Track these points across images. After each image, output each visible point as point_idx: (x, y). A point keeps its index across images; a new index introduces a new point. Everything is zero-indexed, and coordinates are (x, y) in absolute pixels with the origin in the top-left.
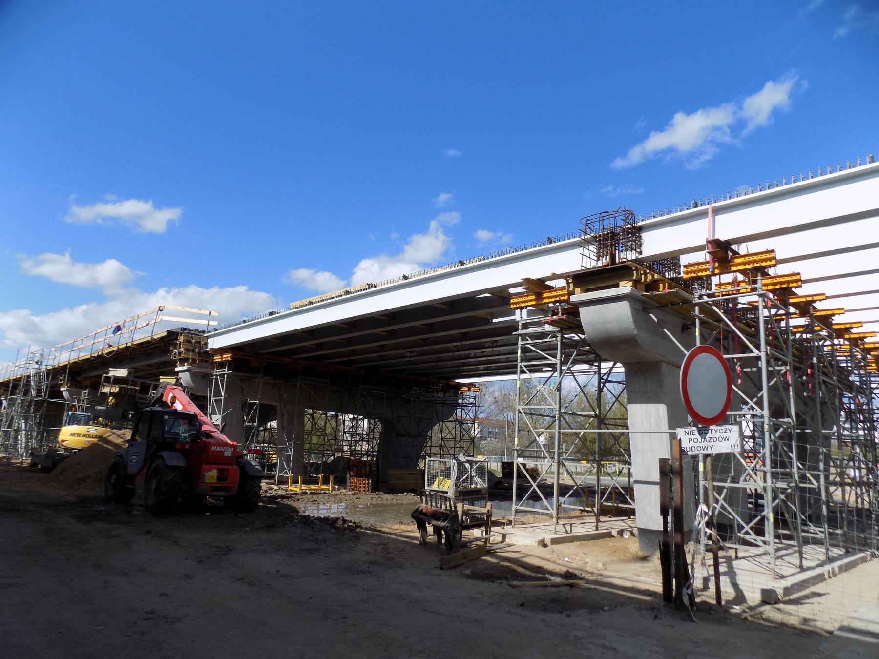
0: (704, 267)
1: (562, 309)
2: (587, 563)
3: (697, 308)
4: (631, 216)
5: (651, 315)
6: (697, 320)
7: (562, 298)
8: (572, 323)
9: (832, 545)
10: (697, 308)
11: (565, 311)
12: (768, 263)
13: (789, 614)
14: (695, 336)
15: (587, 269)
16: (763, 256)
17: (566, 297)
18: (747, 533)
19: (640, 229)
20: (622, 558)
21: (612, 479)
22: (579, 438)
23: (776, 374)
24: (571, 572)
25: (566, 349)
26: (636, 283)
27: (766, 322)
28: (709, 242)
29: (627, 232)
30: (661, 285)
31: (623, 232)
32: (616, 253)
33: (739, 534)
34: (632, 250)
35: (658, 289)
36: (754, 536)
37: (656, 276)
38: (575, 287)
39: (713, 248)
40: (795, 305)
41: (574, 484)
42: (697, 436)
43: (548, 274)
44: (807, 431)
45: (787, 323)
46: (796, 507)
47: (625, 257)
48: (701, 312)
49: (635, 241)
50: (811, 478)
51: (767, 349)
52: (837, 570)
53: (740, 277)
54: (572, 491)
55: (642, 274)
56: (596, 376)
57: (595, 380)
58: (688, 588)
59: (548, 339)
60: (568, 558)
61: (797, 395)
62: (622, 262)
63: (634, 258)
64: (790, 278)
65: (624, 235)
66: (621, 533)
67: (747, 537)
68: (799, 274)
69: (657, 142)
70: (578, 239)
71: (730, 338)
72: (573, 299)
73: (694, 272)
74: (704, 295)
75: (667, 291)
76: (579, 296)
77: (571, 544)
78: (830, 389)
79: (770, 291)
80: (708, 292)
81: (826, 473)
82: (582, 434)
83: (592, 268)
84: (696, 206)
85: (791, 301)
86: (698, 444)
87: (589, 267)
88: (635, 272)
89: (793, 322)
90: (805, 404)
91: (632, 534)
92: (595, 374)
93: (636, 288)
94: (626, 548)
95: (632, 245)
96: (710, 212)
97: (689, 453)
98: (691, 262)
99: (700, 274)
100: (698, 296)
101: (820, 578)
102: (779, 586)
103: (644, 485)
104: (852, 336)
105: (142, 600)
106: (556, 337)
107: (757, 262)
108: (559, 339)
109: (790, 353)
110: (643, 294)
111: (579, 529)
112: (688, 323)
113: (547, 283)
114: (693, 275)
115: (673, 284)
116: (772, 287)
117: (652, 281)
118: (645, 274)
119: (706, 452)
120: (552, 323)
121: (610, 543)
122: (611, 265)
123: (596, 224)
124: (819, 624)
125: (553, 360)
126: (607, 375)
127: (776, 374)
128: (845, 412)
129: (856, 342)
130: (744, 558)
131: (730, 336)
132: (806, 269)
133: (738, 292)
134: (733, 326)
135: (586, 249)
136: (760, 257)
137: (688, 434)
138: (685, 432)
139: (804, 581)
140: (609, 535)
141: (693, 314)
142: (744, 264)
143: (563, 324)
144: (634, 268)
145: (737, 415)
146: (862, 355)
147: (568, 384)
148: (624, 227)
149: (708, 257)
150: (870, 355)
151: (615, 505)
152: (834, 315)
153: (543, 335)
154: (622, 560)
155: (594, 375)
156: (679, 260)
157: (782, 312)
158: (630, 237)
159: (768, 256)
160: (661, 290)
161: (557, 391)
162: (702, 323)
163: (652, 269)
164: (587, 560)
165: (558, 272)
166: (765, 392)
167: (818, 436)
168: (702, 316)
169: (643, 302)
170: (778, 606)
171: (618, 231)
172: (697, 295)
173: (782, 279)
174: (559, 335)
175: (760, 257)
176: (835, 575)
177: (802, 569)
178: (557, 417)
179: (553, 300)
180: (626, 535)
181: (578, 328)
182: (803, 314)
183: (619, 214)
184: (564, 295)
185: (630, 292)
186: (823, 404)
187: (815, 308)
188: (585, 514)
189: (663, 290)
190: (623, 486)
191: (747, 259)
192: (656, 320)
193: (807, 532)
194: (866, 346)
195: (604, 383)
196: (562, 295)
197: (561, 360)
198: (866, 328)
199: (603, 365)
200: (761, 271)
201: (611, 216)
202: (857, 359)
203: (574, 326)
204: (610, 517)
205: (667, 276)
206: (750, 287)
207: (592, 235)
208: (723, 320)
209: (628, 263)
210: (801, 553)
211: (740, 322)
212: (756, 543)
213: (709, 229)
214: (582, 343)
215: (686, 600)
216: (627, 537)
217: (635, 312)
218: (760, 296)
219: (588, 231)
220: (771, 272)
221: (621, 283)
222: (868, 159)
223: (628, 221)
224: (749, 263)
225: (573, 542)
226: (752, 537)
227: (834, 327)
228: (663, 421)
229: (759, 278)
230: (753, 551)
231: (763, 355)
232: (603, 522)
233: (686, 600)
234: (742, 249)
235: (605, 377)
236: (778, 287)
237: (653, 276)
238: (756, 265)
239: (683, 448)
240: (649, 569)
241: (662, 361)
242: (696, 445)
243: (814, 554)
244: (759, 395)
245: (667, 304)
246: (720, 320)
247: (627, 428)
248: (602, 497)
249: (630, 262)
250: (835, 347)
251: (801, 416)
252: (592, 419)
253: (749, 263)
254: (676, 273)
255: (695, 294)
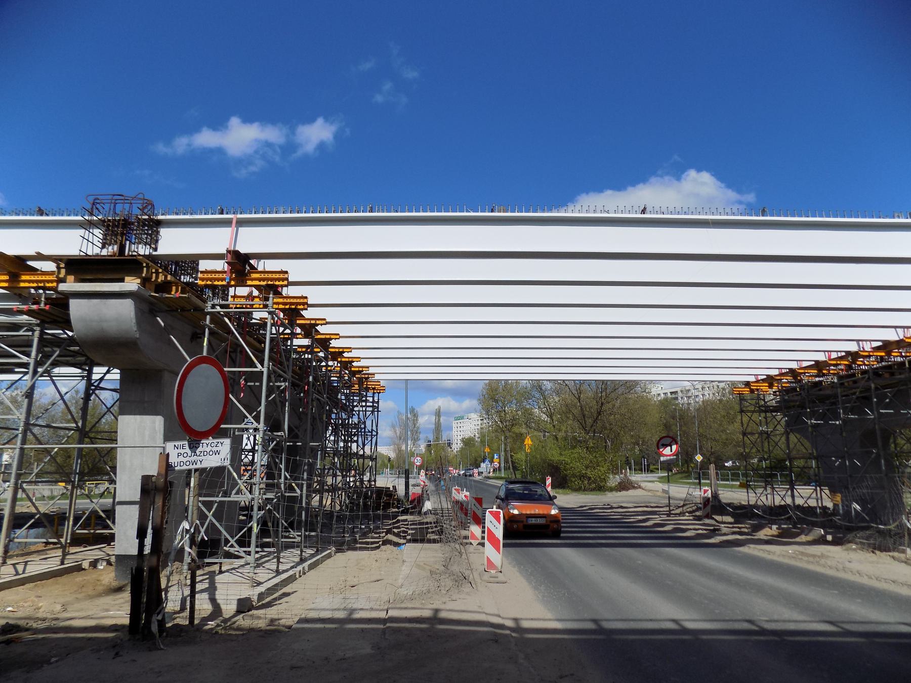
0: (221, 276)
1: (46, 299)
2: (39, 608)
3: (208, 317)
4: (150, 206)
5: (158, 318)
6: (207, 329)
7: (47, 285)
8: (57, 316)
9: (305, 547)
10: (208, 317)
11: (49, 300)
12: (281, 283)
13: (259, 618)
14: (203, 346)
15: (87, 255)
16: (277, 276)
17: (55, 284)
18: (232, 546)
19: (159, 223)
20: (90, 593)
21: (92, 502)
22: (51, 456)
23: (275, 389)
24: (11, 624)
25: (47, 346)
26: (145, 282)
27: (272, 340)
28: (229, 251)
29: (143, 223)
30: (174, 288)
31: (138, 223)
32: (125, 244)
33: (225, 548)
34: (146, 244)
35: (169, 292)
36: (237, 548)
37: (169, 278)
38: (68, 273)
39: (232, 258)
40: (301, 326)
41: (36, 512)
42: (188, 450)
43: (31, 252)
44: (298, 444)
45: (292, 342)
46: (279, 515)
47: (136, 250)
48: (212, 321)
49: (151, 235)
50: (296, 487)
51: (269, 365)
52: (306, 569)
53: (256, 293)
54: (33, 521)
55: (154, 273)
56: (84, 382)
57: (82, 385)
58: (158, 614)
59: (21, 333)
60: (12, 606)
61: (293, 410)
62: (132, 256)
63: (147, 253)
64: (298, 301)
65: (138, 226)
66: (94, 564)
67: (232, 550)
68: (306, 298)
69: (206, 139)
70: (79, 218)
71: (239, 351)
72: (62, 287)
73: (210, 280)
74: (217, 305)
75: (179, 295)
76: (70, 285)
77: (22, 587)
78: (321, 405)
79: (281, 310)
80: (224, 302)
81: (309, 482)
82: (56, 450)
83: (93, 256)
84: (222, 213)
85: (298, 322)
86: (188, 459)
87: (90, 253)
88: (145, 269)
89: (296, 342)
90: (300, 419)
91: (109, 563)
92: (83, 379)
93: (144, 287)
94: (98, 580)
95: (146, 238)
96: (234, 222)
97: (176, 468)
98: (209, 269)
99: (216, 283)
100: (212, 305)
101: (292, 579)
102: (253, 593)
103: (128, 506)
104: (343, 360)
105: (134, 661)
106: (33, 331)
107: (272, 280)
108: (37, 334)
109: (291, 371)
110: (152, 294)
111: (36, 567)
112: (198, 331)
113: (29, 263)
114: (209, 283)
115: (188, 289)
116: (283, 307)
117: (164, 282)
118: (157, 273)
119: (195, 466)
120: (29, 313)
121: (78, 578)
122: (117, 257)
123: (107, 207)
124: (282, 622)
125: (25, 359)
126: (98, 381)
127: (275, 389)
128: (332, 427)
129: (347, 365)
130: (227, 571)
131: (239, 349)
132: (314, 295)
133: (252, 306)
134: (241, 340)
135: (89, 231)
136: (274, 276)
137: (178, 449)
138: (175, 446)
139: (276, 585)
140: (79, 568)
141: (202, 323)
142: (260, 280)
143: (45, 316)
144: (144, 265)
145: (236, 428)
146: (348, 377)
147: (45, 392)
148: (140, 217)
149: (226, 267)
150: (356, 377)
151: (92, 531)
152: (331, 339)
153: (16, 327)
154: (89, 595)
155: (81, 380)
156: (198, 265)
157: (288, 331)
158: (146, 230)
159: (281, 276)
160: (173, 293)
161: (26, 398)
162: (212, 333)
163: (166, 269)
164: (40, 605)
165: (45, 252)
166: (262, 408)
167: (305, 448)
168: (212, 326)
169: (151, 303)
170: (250, 613)
171: (133, 220)
172: (209, 304)
173: (292, 301)
174: (38, 328)
175: (274, 276)
176: (304, 573)
177: (278, 572)
178: (20, 429)
179: (35, 285)
180: (101, 565)
181: (66, 323)
182: (306, 336)
183: (137, 201)
184: (52, 281)
185: (136, 290)
186: (314, 419)
187: (317, 331)
188: (52, 546)
189: (175, 293)
190: (104, 508)
191: (262, 276)
192: (163, 324)
193: (288, 537)
194: (353, 369)
195: (94, 391)
196: (48, 281)
197: (36, 359)
198: (354, 354)
199: (96, 369)
200: (275, 290)
201: (126, 201)
202: (345, 380)
203: (48, 320)
204: (86, 547)
205: (182, 280)
206: (262, 303)
207: (99, 217)
208: (233, 333)
209: (139, 257)
210: (278, 558)
211: (251, 337)
212: (240, 554)
213: (231, 238)
214: (68, 341)
215: (154, 628)
216: (102, 567)
217: (139, 312)
218: (270, 313)
219: (95, 211)
220: (285, 291)
221: (127, 279)
222: (368, 209)
223: (146, 211)
224: (264, 280)
225: (23, 585)
226: (236, 549)
227: (330, 350)
228: (158, 434)
229: (271, 295)
230: (237, 563)
231: (265, 370)
232: (72, 554)
233: (154, 628)
234: (262, 265)
235: (95, 384)
236: (287, 307)
237: (166, 277)
238: (270, 283)
239: (170, 464)
240: (122, 601)
241: (165, 369)
242: (185, 460)
243: (290, 557)
244: (258, 410)
245: (177, 309)
246: (230, 332)
247: (115, 440)
248: (75, 524)
249: (141, 257)
250: (329, 368)
251: (293, 430)
252: (73, 432)
253: (264, 280)
254: (192, 277)
255: (209, 302)
